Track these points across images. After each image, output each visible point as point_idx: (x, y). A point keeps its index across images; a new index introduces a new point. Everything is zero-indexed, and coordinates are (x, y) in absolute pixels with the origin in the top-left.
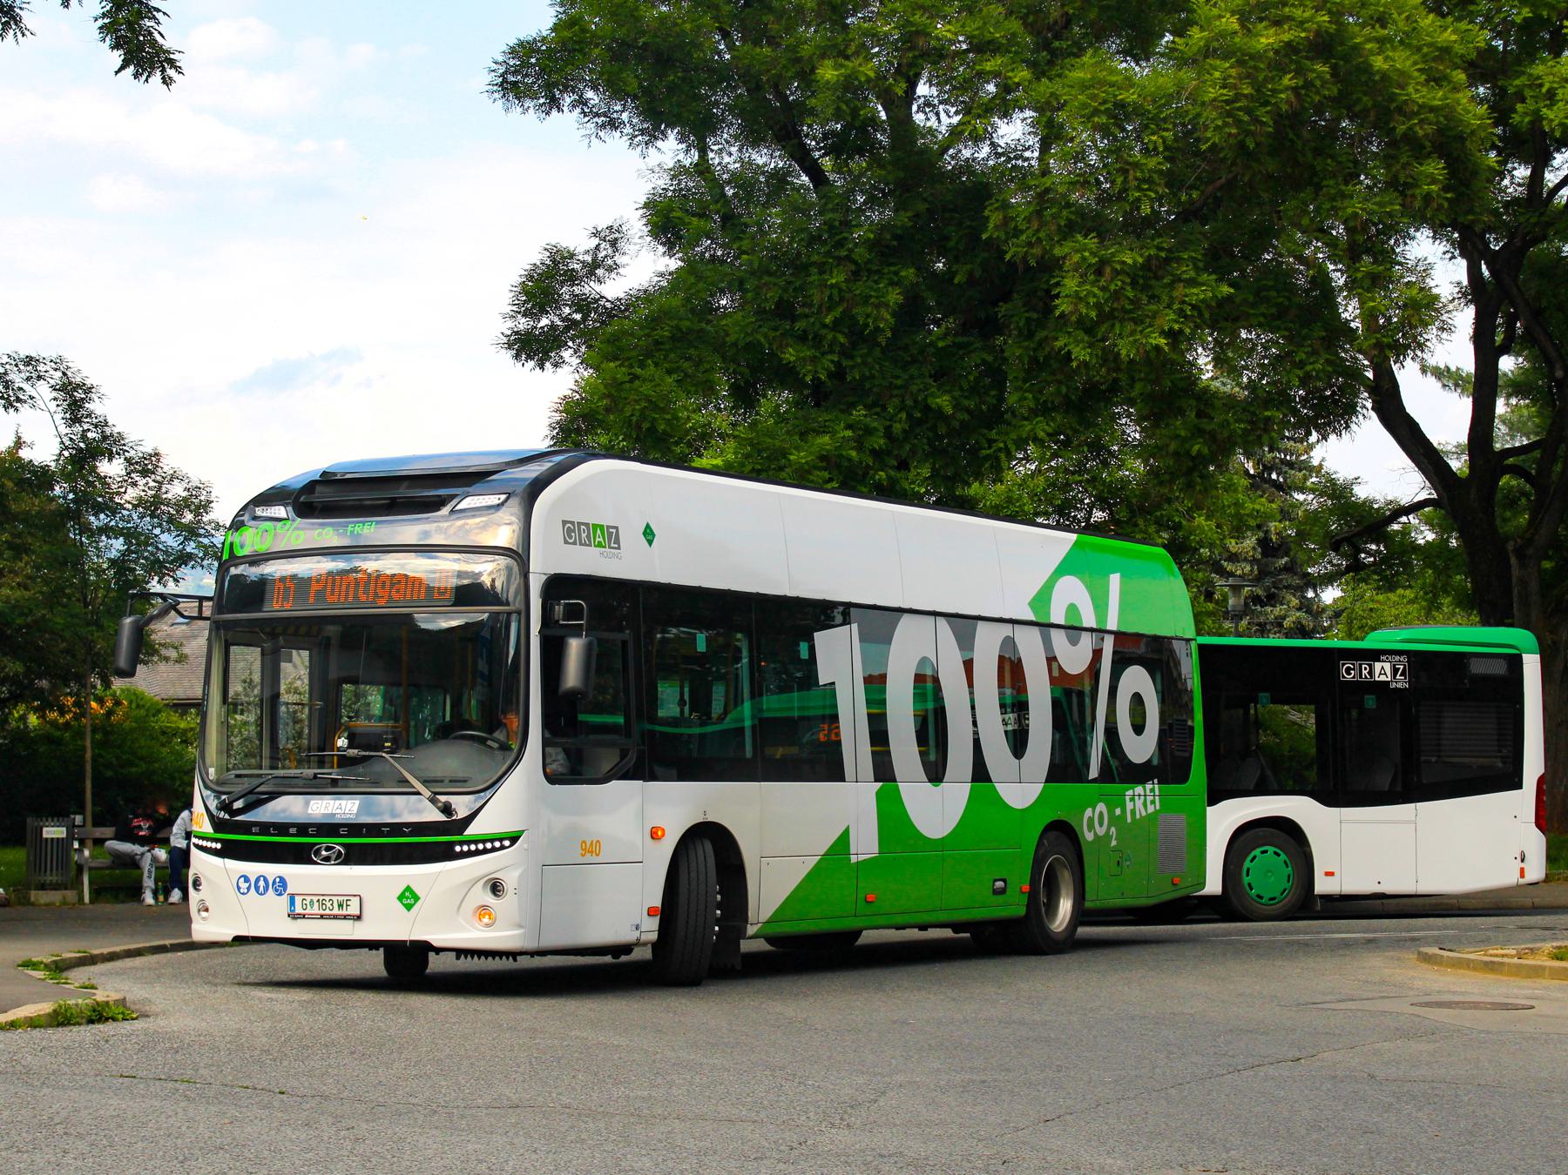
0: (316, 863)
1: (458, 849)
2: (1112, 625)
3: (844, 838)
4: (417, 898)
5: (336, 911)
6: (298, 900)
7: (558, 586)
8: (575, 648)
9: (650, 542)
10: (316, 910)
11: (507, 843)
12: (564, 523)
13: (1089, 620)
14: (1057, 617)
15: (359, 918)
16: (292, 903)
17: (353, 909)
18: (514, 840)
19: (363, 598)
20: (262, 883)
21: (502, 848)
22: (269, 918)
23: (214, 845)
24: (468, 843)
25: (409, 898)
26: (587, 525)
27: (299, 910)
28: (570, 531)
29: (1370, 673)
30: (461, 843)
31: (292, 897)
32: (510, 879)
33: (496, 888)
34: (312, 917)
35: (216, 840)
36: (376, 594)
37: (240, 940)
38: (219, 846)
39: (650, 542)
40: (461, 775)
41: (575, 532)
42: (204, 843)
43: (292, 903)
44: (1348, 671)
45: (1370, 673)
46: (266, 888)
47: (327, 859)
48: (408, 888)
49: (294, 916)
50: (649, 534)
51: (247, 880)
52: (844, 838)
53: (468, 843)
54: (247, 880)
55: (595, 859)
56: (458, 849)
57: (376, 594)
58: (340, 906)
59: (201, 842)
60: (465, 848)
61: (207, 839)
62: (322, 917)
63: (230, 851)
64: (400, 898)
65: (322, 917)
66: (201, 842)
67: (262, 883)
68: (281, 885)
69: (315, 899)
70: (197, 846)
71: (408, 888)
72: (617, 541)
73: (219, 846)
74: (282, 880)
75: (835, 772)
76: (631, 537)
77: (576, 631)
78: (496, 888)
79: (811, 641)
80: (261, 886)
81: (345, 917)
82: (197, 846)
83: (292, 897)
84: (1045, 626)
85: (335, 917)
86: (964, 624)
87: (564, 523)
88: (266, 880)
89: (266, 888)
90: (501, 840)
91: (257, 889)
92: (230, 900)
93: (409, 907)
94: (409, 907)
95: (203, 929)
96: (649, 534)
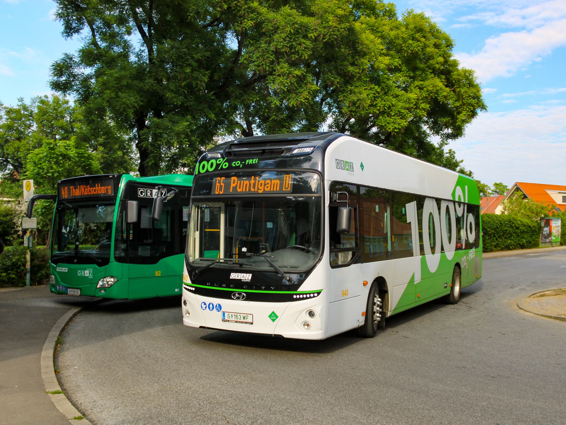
0: (233, 299)
1: (295, 297)
2: (466, 202)
3: (413, 277)
4: (277, 317)
5: (242, 320)
6: (226, 314)
7: (335, 186)
8: (345, 212)
9: (362, 169)
10: (234, 319)
11: (316, 295)
12: (336, 160)
13: (462, 201)
14: (457, 200)
15: (252, 323)
16: (224, 315)
17: (249, 320)
18: (319, 293)
19: (252, 190)
20: (211, 306)
21: (314, 297)
22: (214, 321)
23: (192, 289)
24: (300, 294)
25: (273, 316)
26: (343, 161)
27: (226, 318)
28: (338, 163)
29: (151, 194)
30: (296, 294)
31: (224, 313)
32: (317, 310)
33: (311, 314)
34: (232, 321)
35: (193, 287)
36: (258, 189)
37: (201, 327)
38: (194, 289)
39: (362, 169)
40: (295, 265)
41: (341, 164)
42: (188, 287)
43: (224, 315)
44: (141, 192)
45: (151, 194)
46: (213, 308)
47: (238, 298)
48: (273, 312)
49: (224, 320)
50: (362, 166)
51: (205, 304)
52: (413, 277)
53: (300, 294)
54: (205, 304)
55: (346, 297)
56: (295, 297)
57: (258, 189)
58: (244, 318)
59: (186, 287)
60: (298, 297)
61: (189, 286)
62: (236, 322)
63: (198, 291)
64: (270, 316)
65: (236, 322)
66: (186, 287)
67: (211, 306)
68: (219, 307)
69: (233, 314)
70: (185, 288)
71: (273, 312)
72: (353, 169)
73: (194, 289)
74: (219, 305)
75: (411, 254)
76: (357, 167)
77: (344, 205)
78: (311, 314)
79: (405, 207)
80: (210, 307)
81: (246, 323)
82: (185, 288)
83: (224, 313)
84: (454, 202)
85: (242, 322)
86: (438, 201)
87: (336, 160)
88: (213, 305)
89: (213, 308)
90: (313, 293)
91: (209, 308)
92: (128, 73)
93: (273, 320)
94: (273, 320)
95: (188, 321)
96: (362, 166)
